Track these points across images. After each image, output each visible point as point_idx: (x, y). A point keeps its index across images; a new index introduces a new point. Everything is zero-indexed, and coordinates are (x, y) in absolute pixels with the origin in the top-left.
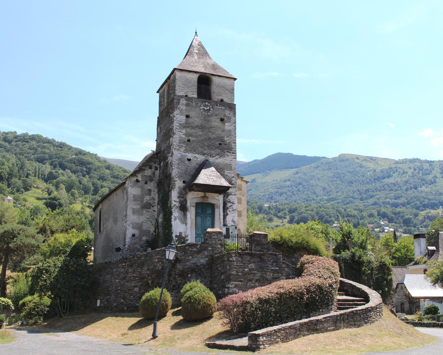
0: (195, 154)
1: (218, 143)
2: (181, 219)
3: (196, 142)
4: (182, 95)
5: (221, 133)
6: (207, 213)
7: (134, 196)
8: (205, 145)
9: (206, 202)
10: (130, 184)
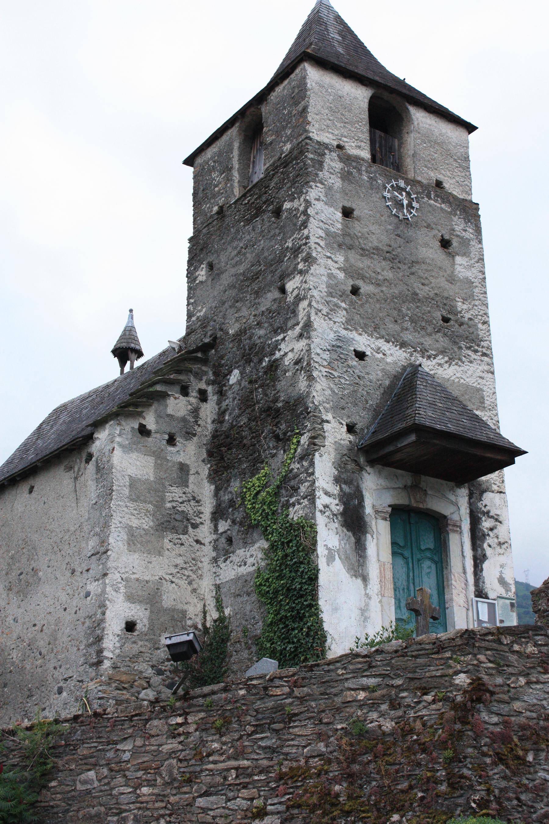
0: (377, 338)
1: (438, 315)
2: (347, 558)
3: (378, 300)
4: (326, 141)
5: (443, 283)
6: (423, 548)
7: (133, 483)
8: (404, 317)
9: (421, 506)
10: (118, 439)
